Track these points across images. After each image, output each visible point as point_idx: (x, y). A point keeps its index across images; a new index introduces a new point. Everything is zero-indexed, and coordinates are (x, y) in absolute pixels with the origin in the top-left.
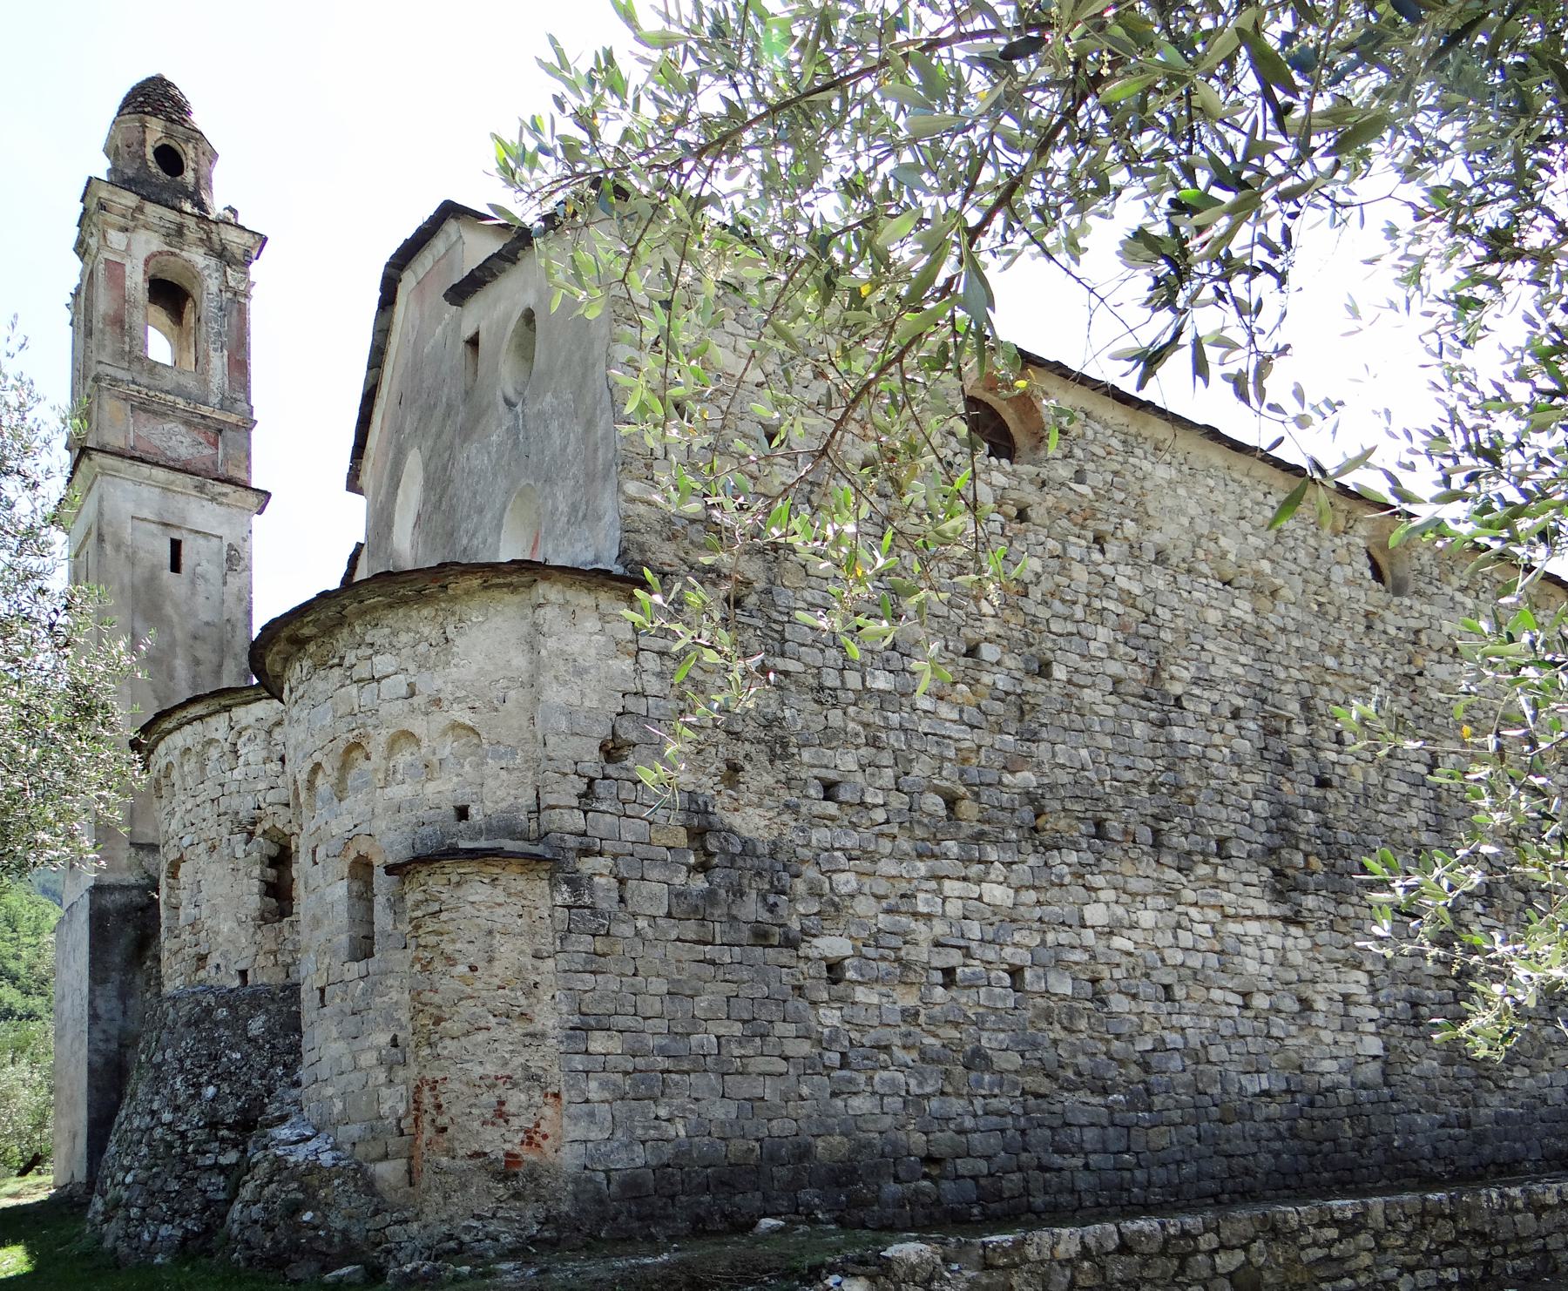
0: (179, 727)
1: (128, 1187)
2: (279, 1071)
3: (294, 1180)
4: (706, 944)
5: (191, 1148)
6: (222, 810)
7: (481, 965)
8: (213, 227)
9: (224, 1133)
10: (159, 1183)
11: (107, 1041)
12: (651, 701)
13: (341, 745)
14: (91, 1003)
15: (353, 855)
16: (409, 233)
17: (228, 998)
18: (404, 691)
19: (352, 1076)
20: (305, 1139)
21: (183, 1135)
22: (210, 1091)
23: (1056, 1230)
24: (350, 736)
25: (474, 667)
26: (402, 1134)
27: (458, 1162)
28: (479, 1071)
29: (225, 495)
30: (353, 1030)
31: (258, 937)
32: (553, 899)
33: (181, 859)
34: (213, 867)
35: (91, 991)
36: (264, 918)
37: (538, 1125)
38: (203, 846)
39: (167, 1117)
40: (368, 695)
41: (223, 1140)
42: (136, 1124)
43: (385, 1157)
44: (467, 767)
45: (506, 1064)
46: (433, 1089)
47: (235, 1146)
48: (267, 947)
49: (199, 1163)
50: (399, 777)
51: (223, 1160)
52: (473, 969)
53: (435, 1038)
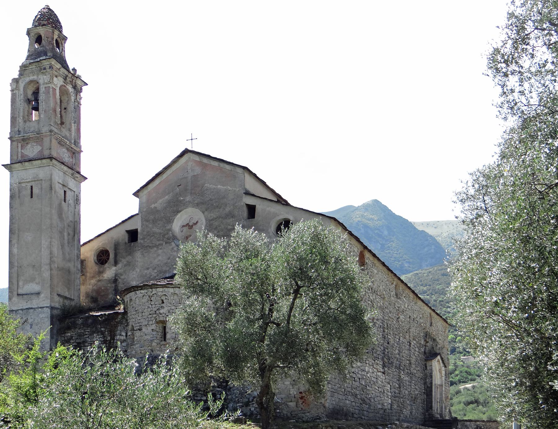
8: (75, 78)
16: (231, 162)
23: (441, 419)
27: (318, 404)
29: (77, 177)
43: (291, 401)
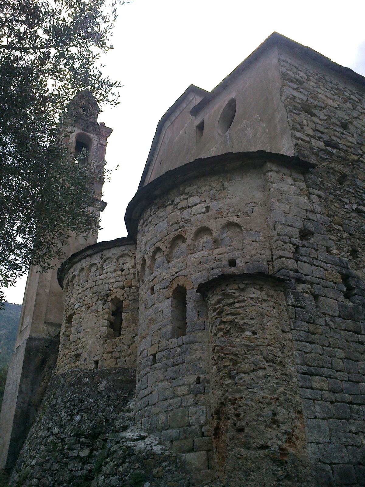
0: (79, 261)
1: (32, 467)
2: (111, 408)
3: (138, 462)
4: (358, 334)
5: (66, 447)
6: (94, 292)
7: (259, 331)
9: (83, 439)
10: (48, 465)
11: (24, 403)
12: (318, 215)
13: (171, 236)
14: (20, 386)
15: (175, 286)
17: (90, 374)
18: (204, 210)
19: (172, 401)
20: (144, 438)
21: (63, 440)
22: (78, 418)
24: (176, 232)
25: (238, 198)
26: (203, 435)
28: (261, 394)
30: (173, 375)
31: (105, 346)
32: (287, 302)
33: (74, 314)
34: (88, 315)
35: (21, 381)
36: (107, 338)
37: (293, 431)
38: (84, 307)
39: (56, 431)
40: (186, 214)
41: (82, 443)
42: (40, 434)
43: (192, 450)
44: (235, 242)
45: (275, 390)
46: (234, 404)
47: (88, 447)
48: (108, 350)
49: (70, 455)
50: (200, 248)
51: (82, 454)
52: (254, 333)
53: (233, 373)
